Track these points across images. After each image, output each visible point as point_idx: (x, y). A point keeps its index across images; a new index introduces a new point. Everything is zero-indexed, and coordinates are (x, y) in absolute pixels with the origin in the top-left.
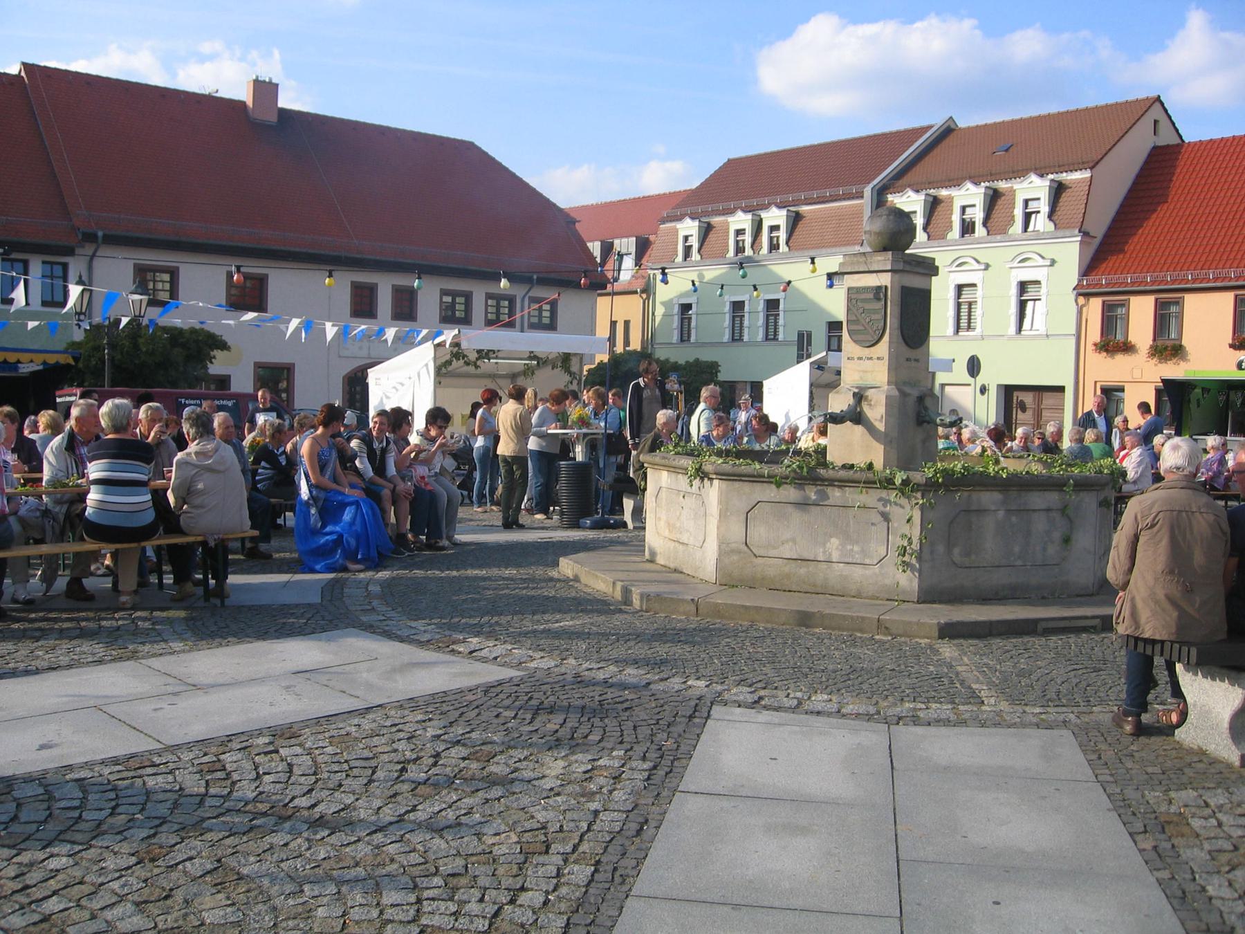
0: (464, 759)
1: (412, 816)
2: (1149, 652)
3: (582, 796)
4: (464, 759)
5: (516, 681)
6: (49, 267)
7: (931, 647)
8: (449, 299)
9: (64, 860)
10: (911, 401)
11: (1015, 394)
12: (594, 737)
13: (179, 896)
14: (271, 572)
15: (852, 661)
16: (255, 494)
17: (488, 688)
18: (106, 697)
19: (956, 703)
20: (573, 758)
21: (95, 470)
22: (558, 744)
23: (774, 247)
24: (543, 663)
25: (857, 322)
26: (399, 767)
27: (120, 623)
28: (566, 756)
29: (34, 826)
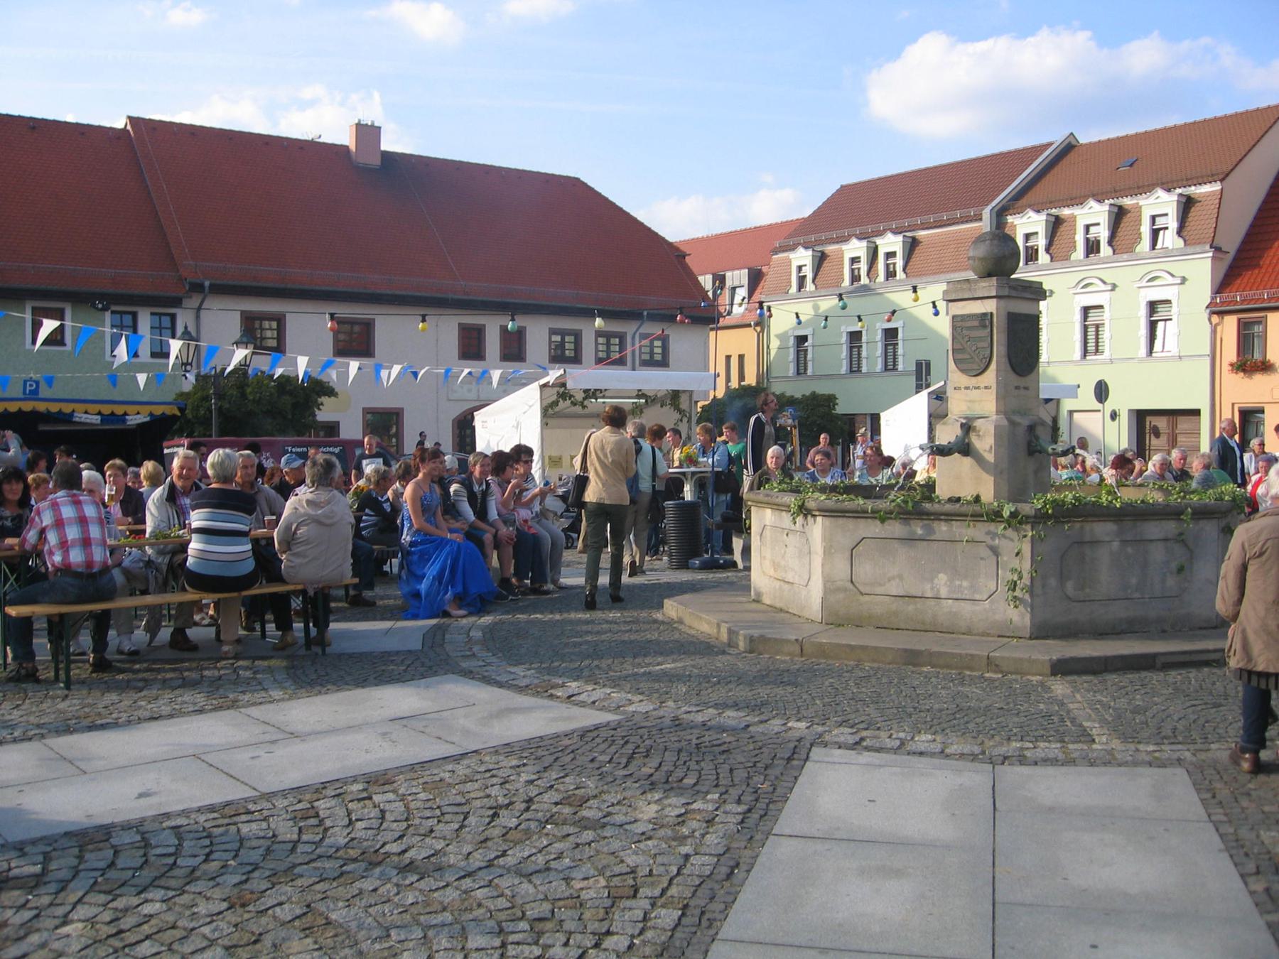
0: (556, 804)
1: (501, 861)
2: (1263, 686)
3: (674, 839)
4: (556, 804)
5: (613, 725)
6: (157, 318)
7: (1042, 684)
8: (558, 338)
9: (158, 905)
10: (1021, 431)
11: (1148, 419)
12: (689, 781)
13: (268, 941)
14: (374, 619)
15: (958, 701)
16: (361, 542)
17: (583, 733)
18: (206, 745)
19: (1064, 741)
20: (666, 802)
21: (197, 519)
22: (653, 786)
23: (890, 274)
24: (641, 706)
25: (962, 350)
26: (491, 812)
27: (222, 672)
28: (660, 800)
29: (130, 873)
